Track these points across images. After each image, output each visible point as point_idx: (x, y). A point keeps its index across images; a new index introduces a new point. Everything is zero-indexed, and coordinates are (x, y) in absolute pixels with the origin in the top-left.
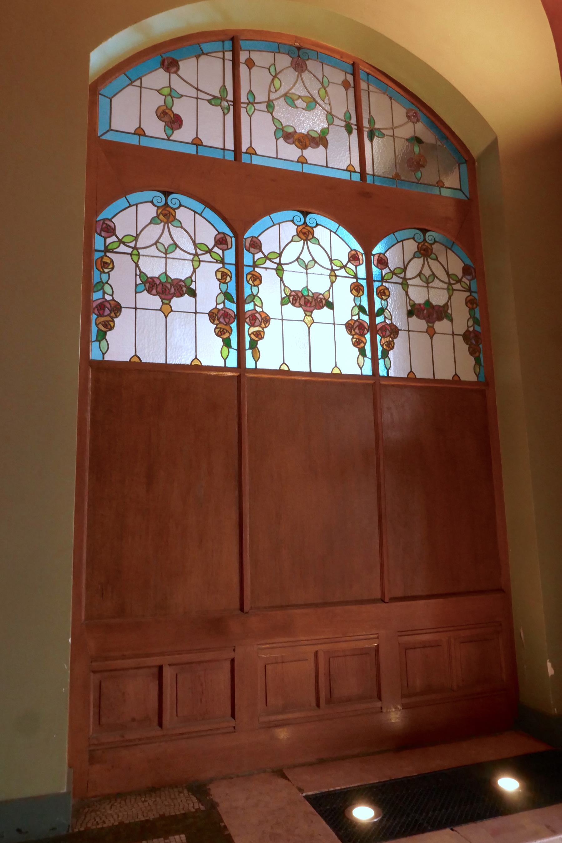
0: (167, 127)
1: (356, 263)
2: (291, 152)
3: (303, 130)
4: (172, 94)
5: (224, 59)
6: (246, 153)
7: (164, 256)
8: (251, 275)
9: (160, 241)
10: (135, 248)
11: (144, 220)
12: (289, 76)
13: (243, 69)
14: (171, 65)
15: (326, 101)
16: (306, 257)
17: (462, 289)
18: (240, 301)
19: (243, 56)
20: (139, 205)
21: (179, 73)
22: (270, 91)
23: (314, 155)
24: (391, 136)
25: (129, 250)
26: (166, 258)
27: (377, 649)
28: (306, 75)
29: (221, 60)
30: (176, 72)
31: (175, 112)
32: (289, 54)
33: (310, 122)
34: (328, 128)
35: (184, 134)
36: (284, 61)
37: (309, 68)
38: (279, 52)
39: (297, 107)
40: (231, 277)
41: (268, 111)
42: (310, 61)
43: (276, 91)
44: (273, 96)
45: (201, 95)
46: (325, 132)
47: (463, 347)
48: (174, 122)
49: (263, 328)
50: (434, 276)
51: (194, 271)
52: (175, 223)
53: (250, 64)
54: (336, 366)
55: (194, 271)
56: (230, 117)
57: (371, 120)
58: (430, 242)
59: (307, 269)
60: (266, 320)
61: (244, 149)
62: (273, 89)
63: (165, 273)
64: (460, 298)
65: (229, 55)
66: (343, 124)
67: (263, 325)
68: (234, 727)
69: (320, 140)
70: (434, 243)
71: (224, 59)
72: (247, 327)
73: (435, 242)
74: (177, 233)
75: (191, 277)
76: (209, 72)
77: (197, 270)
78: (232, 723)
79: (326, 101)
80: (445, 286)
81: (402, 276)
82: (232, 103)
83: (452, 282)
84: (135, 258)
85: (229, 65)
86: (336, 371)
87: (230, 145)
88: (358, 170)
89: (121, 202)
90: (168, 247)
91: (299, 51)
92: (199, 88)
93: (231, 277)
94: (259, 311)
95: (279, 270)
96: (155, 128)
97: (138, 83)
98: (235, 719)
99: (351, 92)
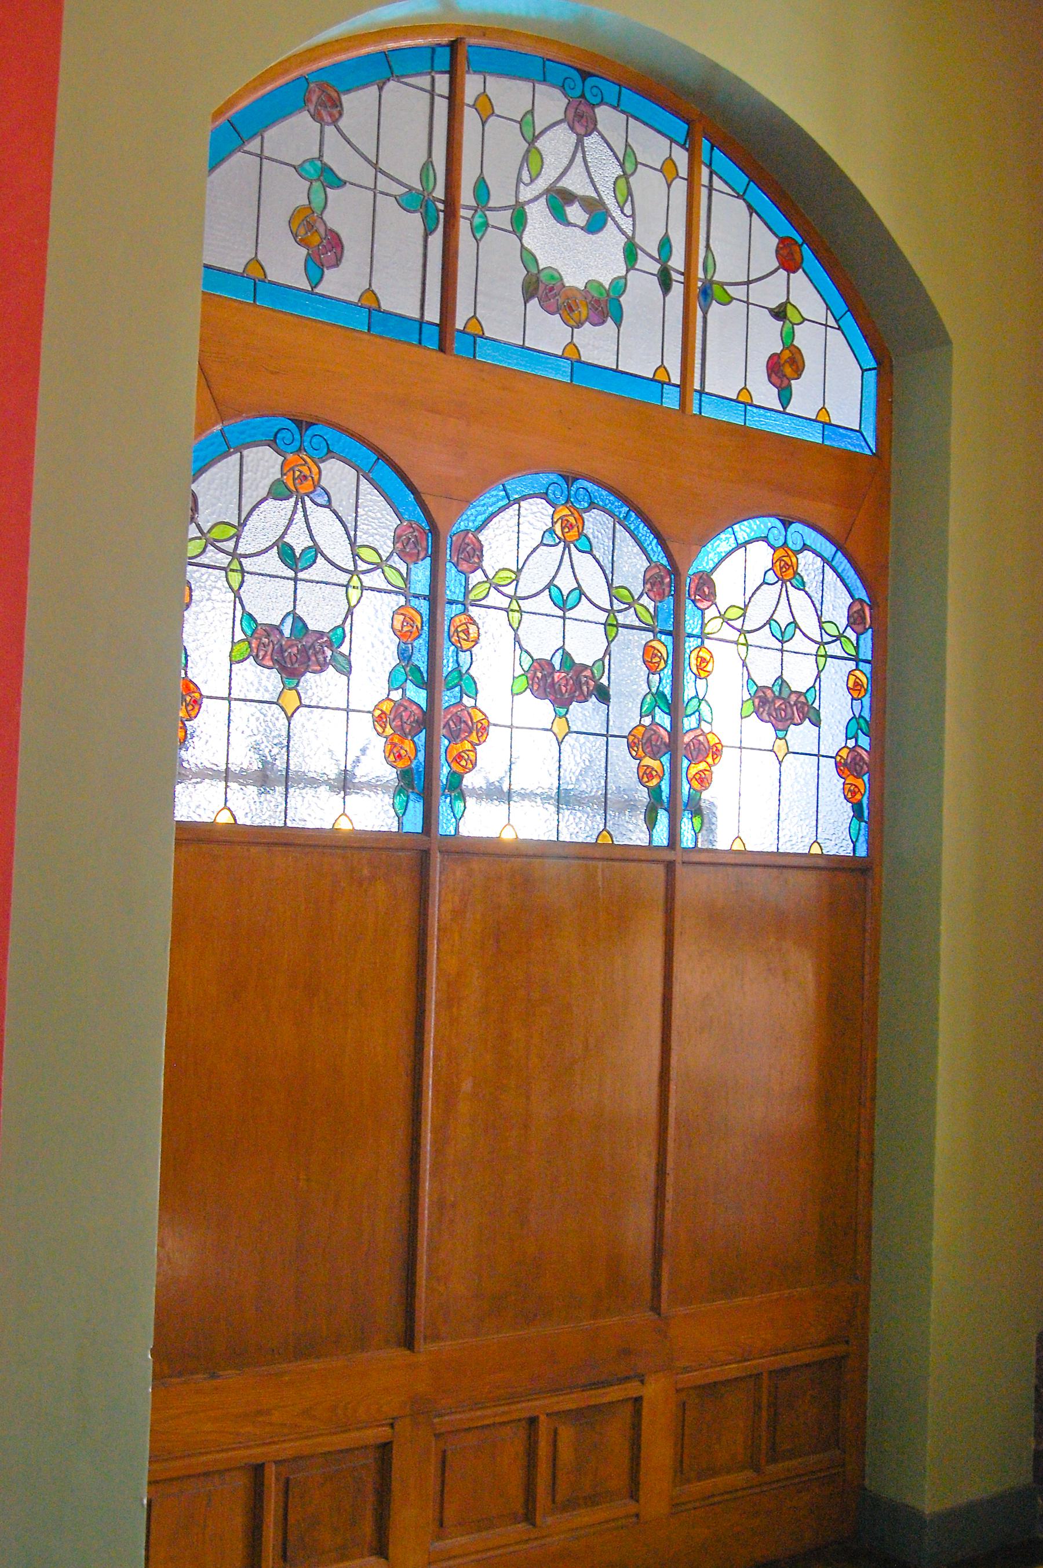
0: (310, 263)
1: (859, 628)
2: (548, 333)
3: (574, 279)
4: (328, 178)
5: (432, 93)
6: (463, 332)
7: (778, 645)
8: (402, 617)
9: (555, 582)
10: (234, 554)
11: (532, 537)
12: (557, 144)
13: (470, 119)
14: (328, 106)
15: (628, 210)
16: (565, 582)
17: (384, 585)
18: (674, 706)
19: (472, 86)
20: (748, 546)
21: (341, 124)
22: (519, 180)
23: (596, 344)
24: (256, 155)
25: (504, 602)
26: (295, 580)
27: (385, 1449)
28: (592, 142)
29: (427, 96)
30: (335, 122)
31: (330, 225)
32: (562, 88)
33: (584, 260)
34: (625, 278)
35: (341, 283)
36: (551, 104)
37: (599, 127)
38: (544, 81)
39: (569, 224)
40: (666, 662)
41: (514, 232)
42: (603, 107)
43: (532, 181)
44: (526, 193)
45: (383, 183)
46: (620, 285)
47: (833, 784)
48: (324, 249)
49: (710, 766)
50: (316, 550)
51: (350, 612)
52: (582, 543)
53: (486, 110)
54: (344, 814)
55: (350, 612)
56: (436, 240)
57: (481, 187)
58: (794, 548)
59: (782, 642)
60: (716, 752)
61: (459, 325)
62: (526, 177)
63: (562, 648)
64: (837, 673)
65: (442, 83)
66: (655, 268)
67: (710, 760)
68: (637, 1515)
69: (603, 306)
70: (801, 551)
71: (432, 93)
72: (685, 763)
73: (805, 547)
74: (584, 563)
75: (342, 626)
76: (397, 122)
77: (747, 661)
78: (632, 1507)
79: (628, 210)
80: (602, 617)
81: (229, 545)
82: (681, 278)
83: (827, 638)
84: (235, 578)
85: (442, 106)
86: (738, 846)
88: (676, 379)
89: (493, 497)
90: (316, 557)
91: (584, 80)
92: (382, 165)
93: (666, 662)
94: (468, 705)
96: (286, 265)
97: (254, 146)
98: (387, 1558)
99: (680, 187)
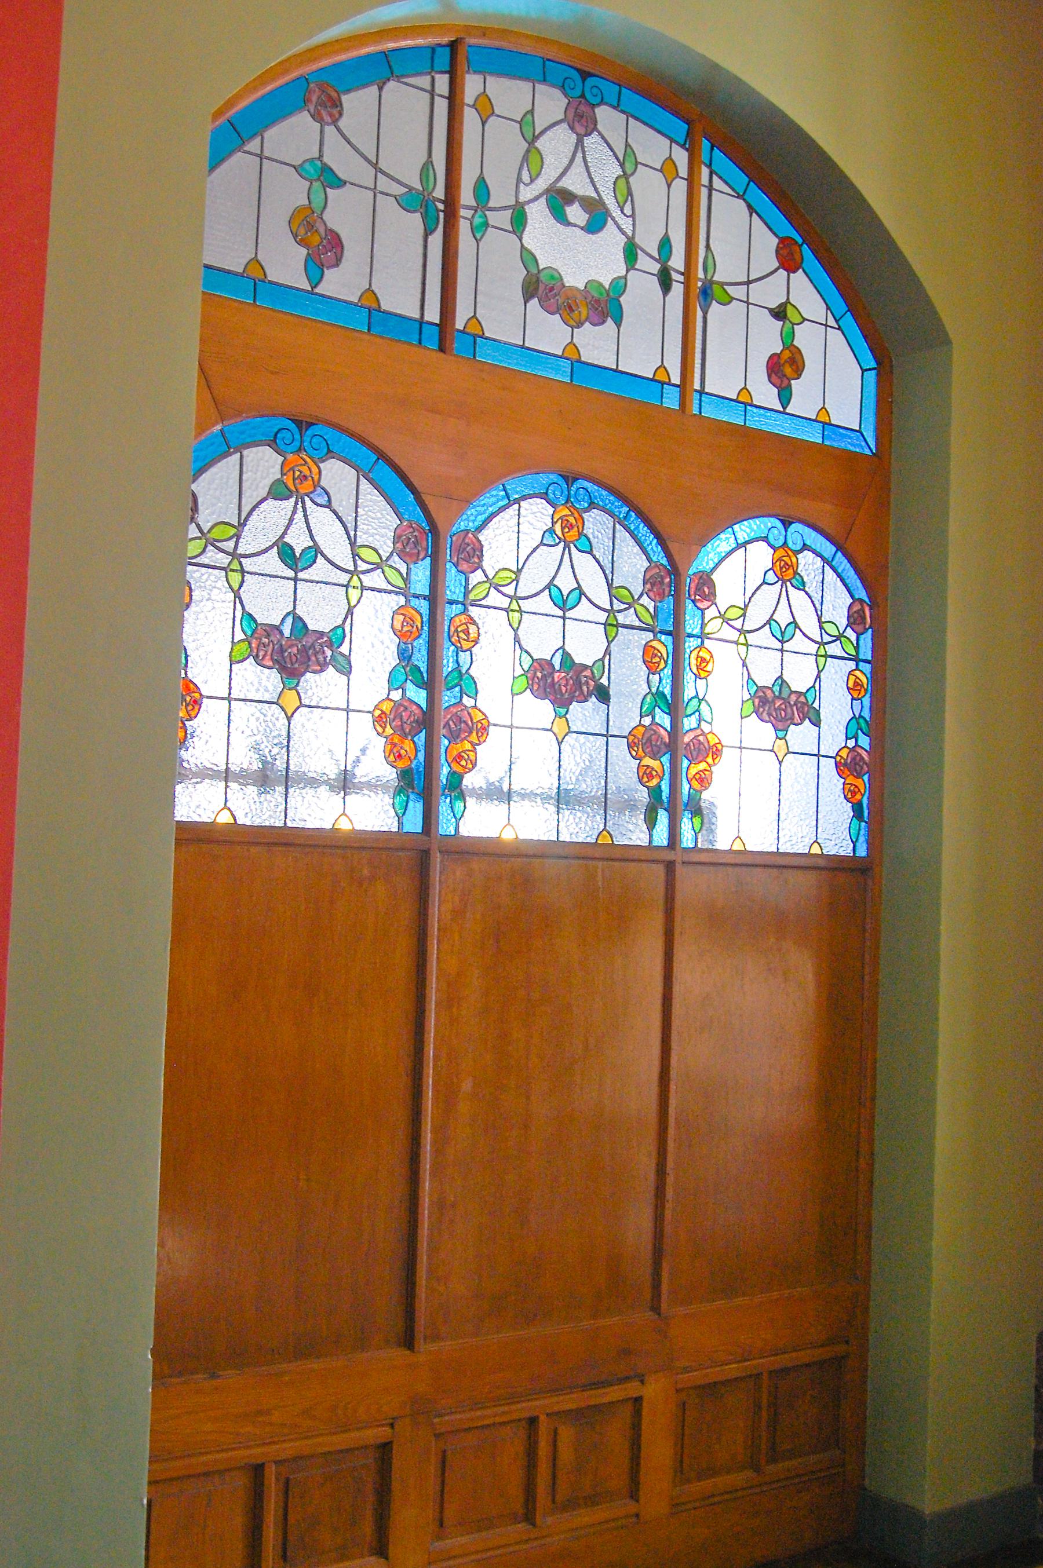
0: (310, 263)
1: (859, 628)
2: (548, 333)
3: (574, 279)
4: (328, 178)
5: (432, 93)
6: (463, 332)
7: (778, 645)
8: (402, 617)
9: (555, 582)
10: (234, 554)
11: (532, 537)
12: (557, 144)
13: (470, 119)
14: (328, 106)
15: (628, 210)
16: (565, 582)
17: (384, 585)
19: (472, 86)
20: (748, 546)
21: (341, 124)
22: (519, 180)
23: (596, 344)
25: (504, 602)
26: (295, 580)
28: (592, 142)
29: (427, 96)
30: (335, 122)
31: (330, 225)
32: (562, 88)
33: (584, 260)
34: (625, 278)
35: (341, 283)
36: (551, 104)
37: (599, 127)
38: (544, 81)
39: (569, 224)
40: (666, 662)
41: (514, 232)
42: (603, 107)
43: (532, 181)
44: (526, 193)
45: (383, 183)
46: (620, 285)
47: (833, 784)
48: (324, 249)
49: (710, 766)
50: (316, 550)
51: (350, 612)
52: (582, 543)
53: (486, 110)
55: (350, 612)
56: (436, 240)
58: (794, 548)
59: (782, 642)
60: (716, 752)
61: (459, 325)
62: (526, 177)
64: (837, 673)
65: (442, 83)
66: (655, 268)
67: (710, 760)
68: (637, 1515)
69: (603, 306)
70: (801, 551)
71: (432, 93)
72: (685, 763)
73: (805, 547)
74: (584, 563)
75: (342, 626)
76: (397, 122)
78: (632, 1507)
79: (628, 210)
80: (602, 617)
81: (229, 545)
83: (827, 638)
84: (235, 578)
85: (442, 106)
86: (738, 846)
87: (433, 315)
88: (676, 379)
89: (493, 497)
90: (316, 557)
91: (584, 80)
92: (382, 165)
93: (666, 662)
94: (468, 705)
95: (236, 566)
96: (286, 265)
97: (254, 146)
99: (680, 187)
